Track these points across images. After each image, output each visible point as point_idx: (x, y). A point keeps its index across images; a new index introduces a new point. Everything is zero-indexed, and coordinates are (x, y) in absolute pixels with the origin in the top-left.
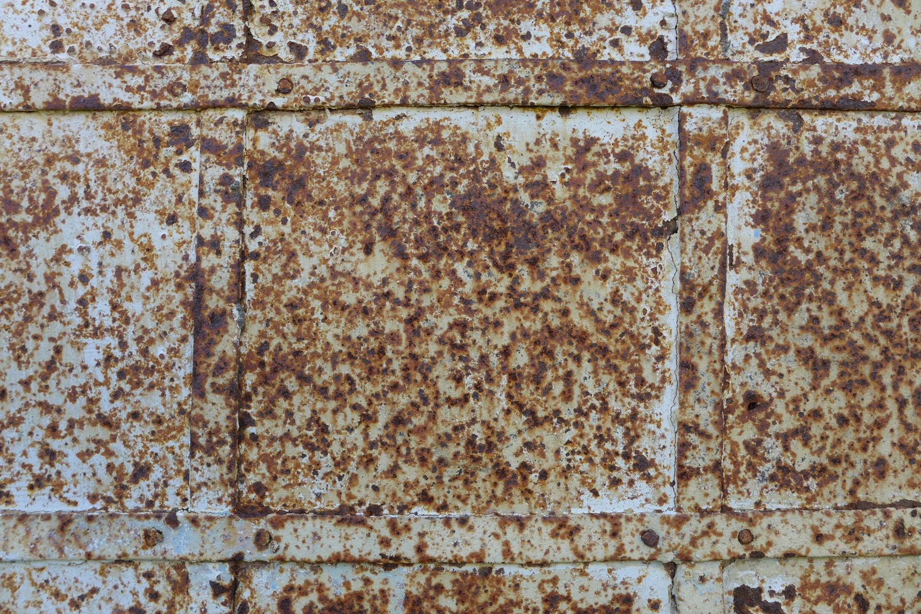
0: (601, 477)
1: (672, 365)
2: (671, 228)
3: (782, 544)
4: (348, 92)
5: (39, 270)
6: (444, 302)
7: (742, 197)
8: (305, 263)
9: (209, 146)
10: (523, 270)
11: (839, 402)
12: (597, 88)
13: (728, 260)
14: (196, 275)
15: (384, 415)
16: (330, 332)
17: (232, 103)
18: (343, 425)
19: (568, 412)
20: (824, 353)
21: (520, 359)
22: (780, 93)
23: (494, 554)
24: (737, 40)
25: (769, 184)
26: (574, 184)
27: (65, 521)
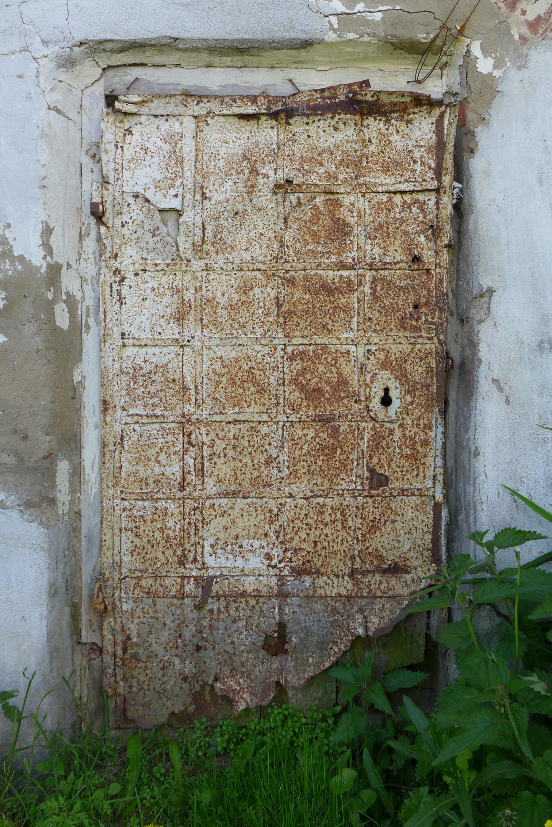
0: (344, 331)
1: (356, 313)
2: (356, 290)
3: (374, 342)
4: (302, 267)
5: (251, 297)
6: (318, 302)
7: (368, 285)
8: (295, 296)
9: (279, 276)
10: (331, 297)
11: (384, 319)
12: (343, 266)
13: (365, 295)
14: (277, 298)
15: (309, 321)
16: (300, 307)
17: (283, 269)
18: (302, 323)
19: (339, 320)
20: (382, 310)
21: (331, 311)
22: (374, 267)
23: (327, 343)
24: (367, 258)
25: (373, 282)
26: (340, 283)
27: (257, 338)
